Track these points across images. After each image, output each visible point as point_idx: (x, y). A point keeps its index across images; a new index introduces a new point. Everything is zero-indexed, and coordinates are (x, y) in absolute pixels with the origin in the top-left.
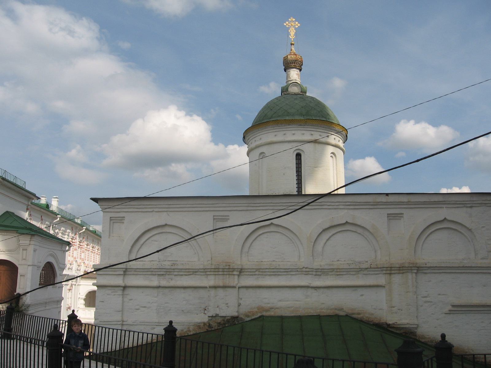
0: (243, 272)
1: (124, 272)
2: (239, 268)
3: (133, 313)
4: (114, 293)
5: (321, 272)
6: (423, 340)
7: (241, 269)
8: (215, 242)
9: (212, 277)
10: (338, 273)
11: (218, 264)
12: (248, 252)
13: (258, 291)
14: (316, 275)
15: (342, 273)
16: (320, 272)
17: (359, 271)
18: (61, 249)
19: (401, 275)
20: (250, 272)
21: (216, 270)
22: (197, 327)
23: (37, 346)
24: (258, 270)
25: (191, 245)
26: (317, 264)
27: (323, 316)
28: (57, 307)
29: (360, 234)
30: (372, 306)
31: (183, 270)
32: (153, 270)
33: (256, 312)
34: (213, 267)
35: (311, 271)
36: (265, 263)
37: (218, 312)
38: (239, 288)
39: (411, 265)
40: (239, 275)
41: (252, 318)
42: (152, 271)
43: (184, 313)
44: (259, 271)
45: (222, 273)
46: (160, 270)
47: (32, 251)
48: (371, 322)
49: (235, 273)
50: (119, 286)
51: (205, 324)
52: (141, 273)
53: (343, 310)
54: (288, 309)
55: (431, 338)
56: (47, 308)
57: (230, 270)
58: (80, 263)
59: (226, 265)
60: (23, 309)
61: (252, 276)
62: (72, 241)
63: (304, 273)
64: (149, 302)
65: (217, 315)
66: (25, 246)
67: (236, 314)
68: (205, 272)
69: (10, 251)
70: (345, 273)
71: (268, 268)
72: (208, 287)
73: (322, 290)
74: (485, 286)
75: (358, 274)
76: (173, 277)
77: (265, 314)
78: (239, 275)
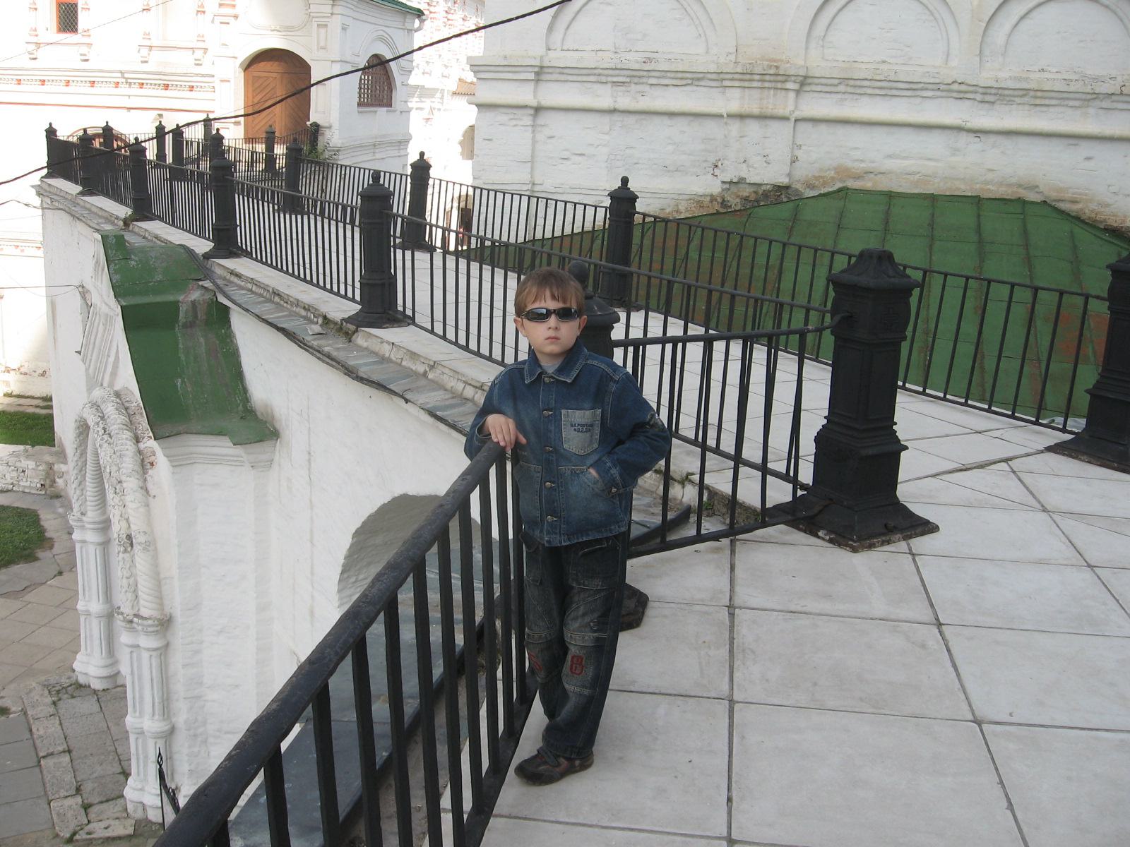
0: (810, 84)
1: (537, 74)
2: (801, 74)
3: (555, 167)
4: (514, 122)
5: (995, 94)
7: (806, 77)
8: (748, 9)
9: (736, 93)
10: (1038, 102)
11: (750, 62)
12: (824, 37)
13: (841, 131)
14: (982, 102)
15: (1047, 102)
16: (994, 95)
17: (1089, 100)
18: (404, 25)
20: (826, 85)
21: (746, 78)
22: (695, 204)
23: (333, 223)
24: (844, 80)
25: (689, 15)
26: (990, 74)
27: (987, 199)
28: (399, 154)
29: (1107, 7)
30: (1109, 186)
31: (669, 74)
32: (601, 71)
33: (833, 178)
34: (739, 70)
35: (971, 92)
36: (863, 66)
37: (744, 173)
38: (796, 121)
40: (798, 92)
41: (822, 192)
42: (599, 75)
43: (669, 171)
44: (847, 85)
45: (759, 84)
46: (617, 72)
47: (339, 30)
48: (1101, 222)
49: (790, 85)
50: (525, 107)
51: (713, 198)
52: (575, 78)
53: (1037, 190)
54: (908, 177)
56: (378, 156)
57: (780, 78)
58: (449, 60)
59: (770, 67)
60: (327, 157)
61: (828, 95)
62: (428, 10)
63: (955, 95)
64: (592, 145)
65: (741, 181)
66: (324, 17)
67: (784, 180)
68: (720, 79)
69: (287, 29)
70: (1053, 102)
71: (870, 78)
72: (725, 116)
73: (992, 139)
75: (1088, 106)
76: (647, 88)
77: (851, 184)
78: (798, 92)
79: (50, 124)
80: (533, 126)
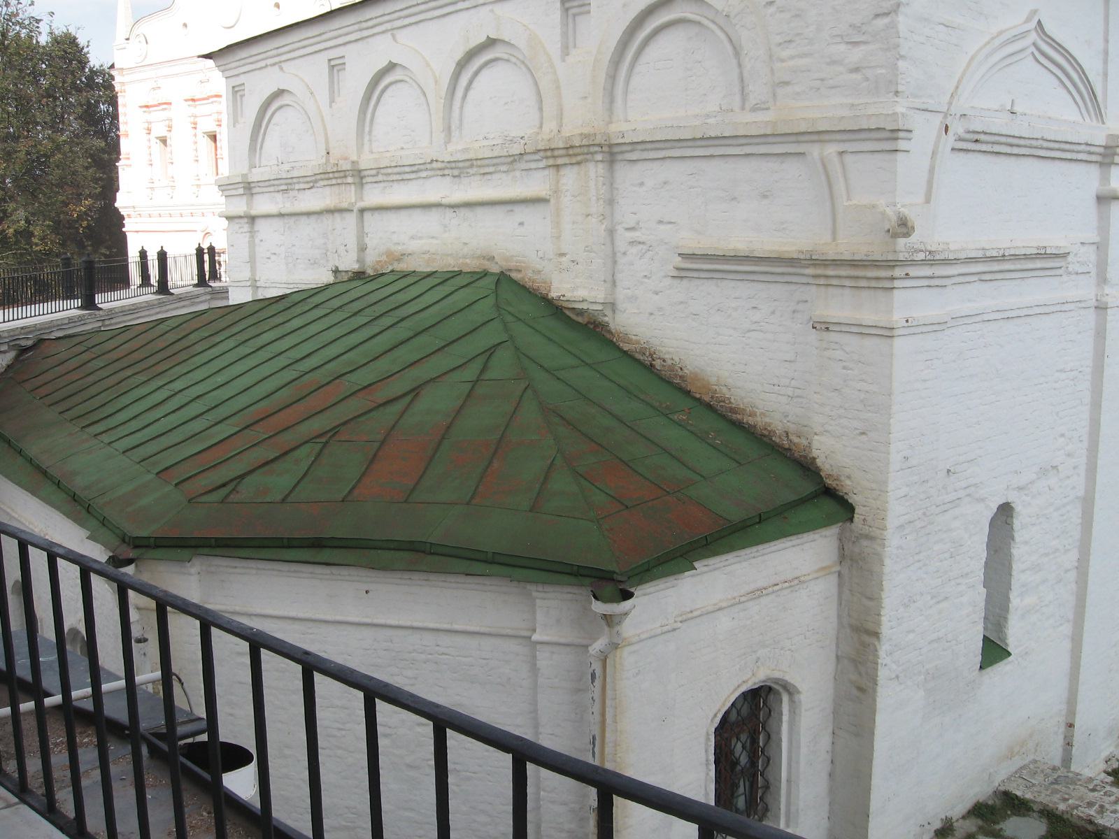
6: (626, 347)
16: (458, 169)
19: (576, 168)
26: (455, 149)
39: (585, 142)
49: (350, 180)
55: (642, 342)
74: (765, 197)
79: (143, 247)
80: (250, 232)
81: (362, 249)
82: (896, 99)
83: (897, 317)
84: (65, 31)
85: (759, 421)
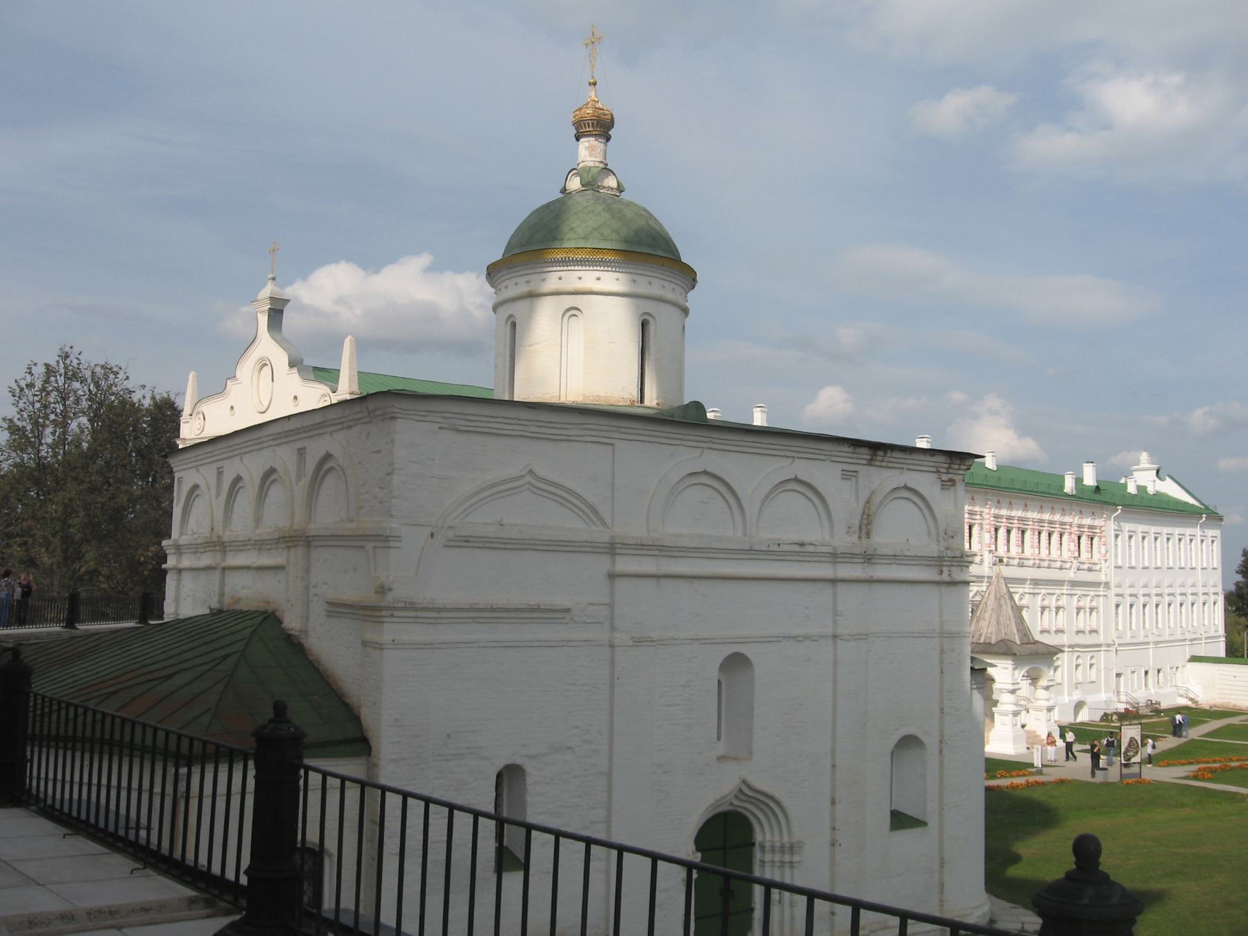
6: (311, 658)
49: (218, 548)
81: (222, 594)
82: (391, 519)
83: (387, 638)
84: (165, 395)
85: (349, 701)
